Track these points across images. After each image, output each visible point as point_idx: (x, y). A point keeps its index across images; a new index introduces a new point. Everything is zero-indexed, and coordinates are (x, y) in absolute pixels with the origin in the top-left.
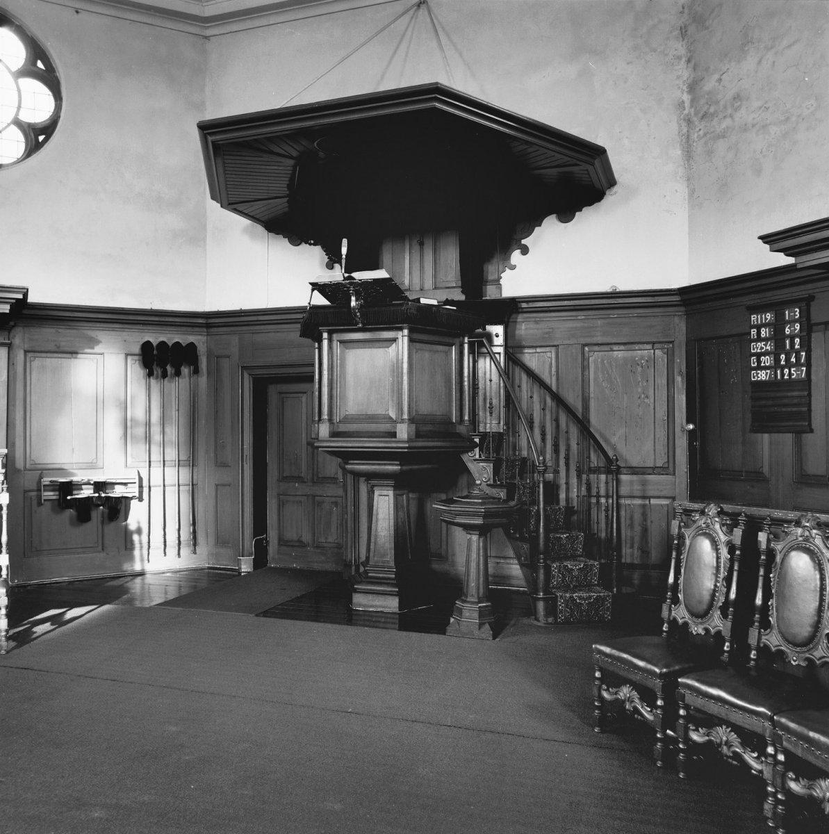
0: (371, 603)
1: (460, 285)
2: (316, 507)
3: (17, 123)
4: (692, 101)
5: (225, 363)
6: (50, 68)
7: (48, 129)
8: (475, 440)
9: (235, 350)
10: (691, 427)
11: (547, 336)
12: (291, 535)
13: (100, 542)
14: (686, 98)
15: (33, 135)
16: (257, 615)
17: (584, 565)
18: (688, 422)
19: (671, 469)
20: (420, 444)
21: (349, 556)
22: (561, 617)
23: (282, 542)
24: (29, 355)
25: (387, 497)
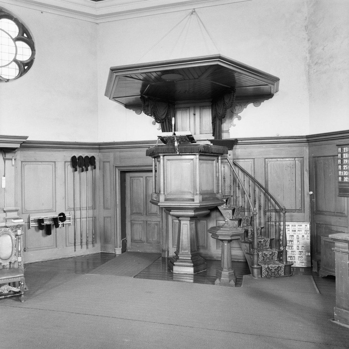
0: (182, 270)
1: (212, 132)
2: (148, 226)
3: (15, 61)
4: (311, 57)
5: (107, 165)
6: (29, 37)
7: (29, 64)
8: (224, 200)
9: (112, 159)
10: (311, 193)
11: (249, 154)
12: (137, 237)
13: (55, 244)
14: (308, 55)
15: (22, 66)
16: (134, 277)
17: (272, 253)
18: (310, 191)
19: (303, 210)
20: (204, 204)
21: (164, 247)
22: (264, 275)
23: (133, 240)
24: (23, 163)
25: (106, 218)
